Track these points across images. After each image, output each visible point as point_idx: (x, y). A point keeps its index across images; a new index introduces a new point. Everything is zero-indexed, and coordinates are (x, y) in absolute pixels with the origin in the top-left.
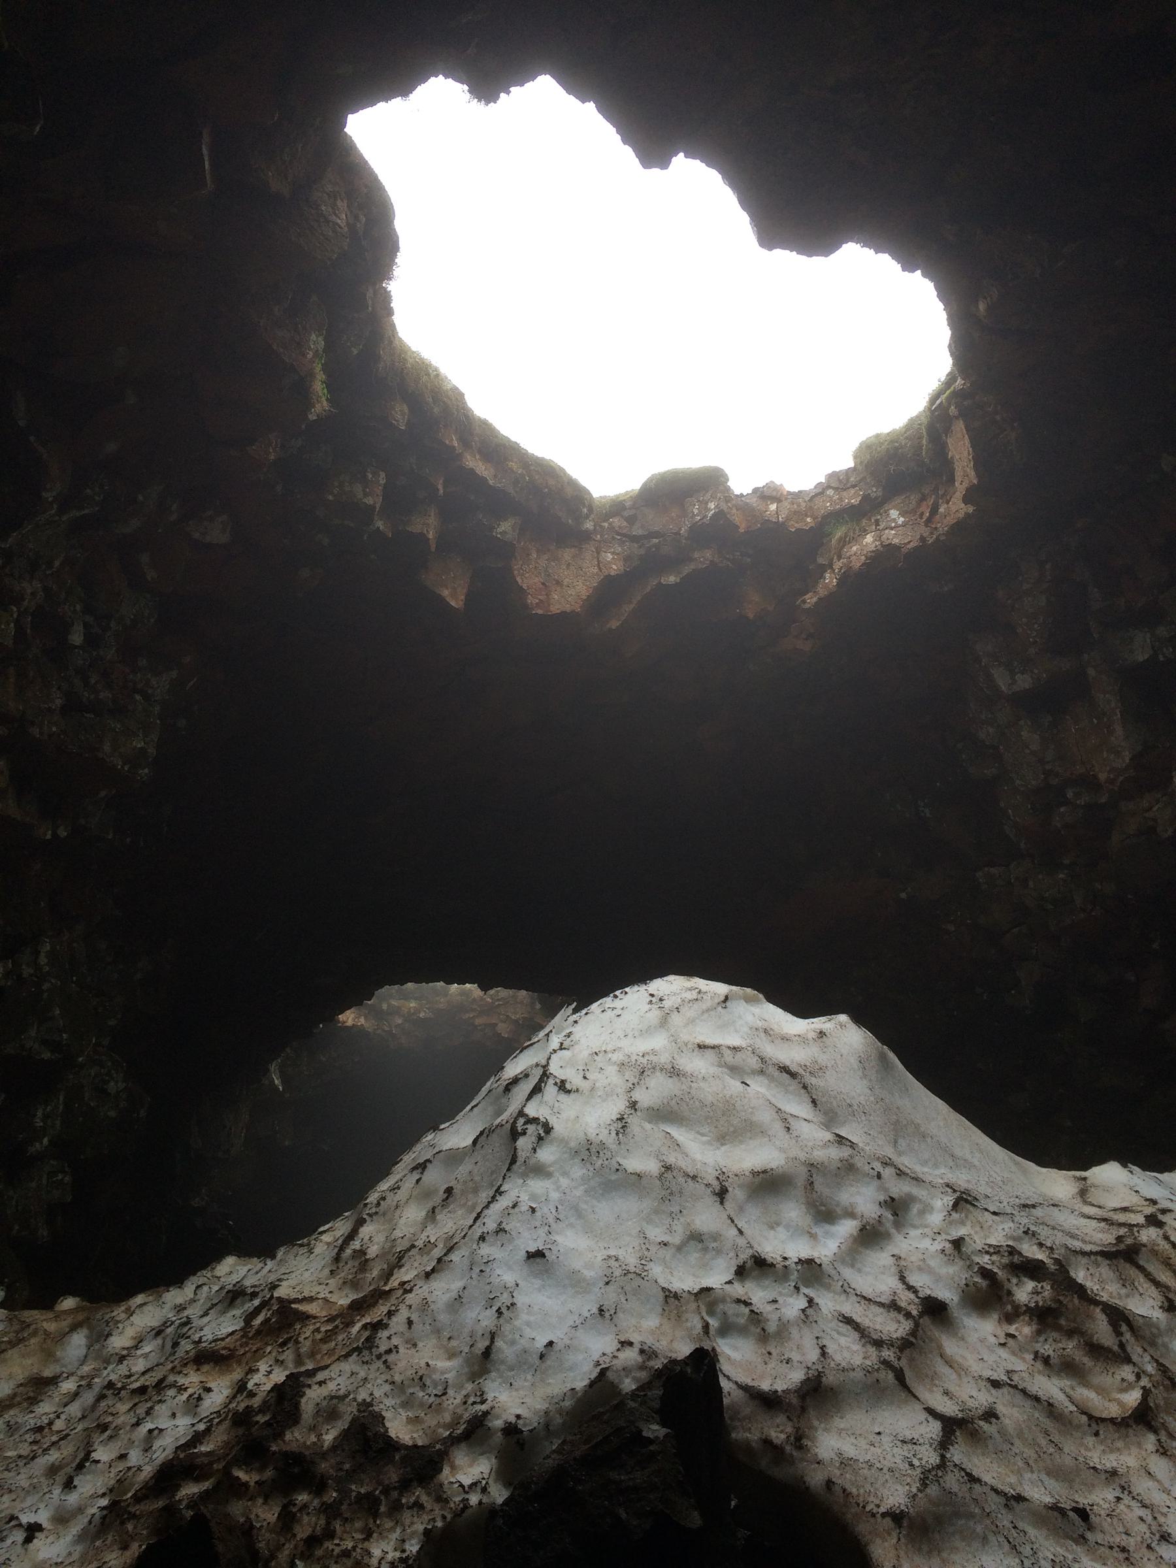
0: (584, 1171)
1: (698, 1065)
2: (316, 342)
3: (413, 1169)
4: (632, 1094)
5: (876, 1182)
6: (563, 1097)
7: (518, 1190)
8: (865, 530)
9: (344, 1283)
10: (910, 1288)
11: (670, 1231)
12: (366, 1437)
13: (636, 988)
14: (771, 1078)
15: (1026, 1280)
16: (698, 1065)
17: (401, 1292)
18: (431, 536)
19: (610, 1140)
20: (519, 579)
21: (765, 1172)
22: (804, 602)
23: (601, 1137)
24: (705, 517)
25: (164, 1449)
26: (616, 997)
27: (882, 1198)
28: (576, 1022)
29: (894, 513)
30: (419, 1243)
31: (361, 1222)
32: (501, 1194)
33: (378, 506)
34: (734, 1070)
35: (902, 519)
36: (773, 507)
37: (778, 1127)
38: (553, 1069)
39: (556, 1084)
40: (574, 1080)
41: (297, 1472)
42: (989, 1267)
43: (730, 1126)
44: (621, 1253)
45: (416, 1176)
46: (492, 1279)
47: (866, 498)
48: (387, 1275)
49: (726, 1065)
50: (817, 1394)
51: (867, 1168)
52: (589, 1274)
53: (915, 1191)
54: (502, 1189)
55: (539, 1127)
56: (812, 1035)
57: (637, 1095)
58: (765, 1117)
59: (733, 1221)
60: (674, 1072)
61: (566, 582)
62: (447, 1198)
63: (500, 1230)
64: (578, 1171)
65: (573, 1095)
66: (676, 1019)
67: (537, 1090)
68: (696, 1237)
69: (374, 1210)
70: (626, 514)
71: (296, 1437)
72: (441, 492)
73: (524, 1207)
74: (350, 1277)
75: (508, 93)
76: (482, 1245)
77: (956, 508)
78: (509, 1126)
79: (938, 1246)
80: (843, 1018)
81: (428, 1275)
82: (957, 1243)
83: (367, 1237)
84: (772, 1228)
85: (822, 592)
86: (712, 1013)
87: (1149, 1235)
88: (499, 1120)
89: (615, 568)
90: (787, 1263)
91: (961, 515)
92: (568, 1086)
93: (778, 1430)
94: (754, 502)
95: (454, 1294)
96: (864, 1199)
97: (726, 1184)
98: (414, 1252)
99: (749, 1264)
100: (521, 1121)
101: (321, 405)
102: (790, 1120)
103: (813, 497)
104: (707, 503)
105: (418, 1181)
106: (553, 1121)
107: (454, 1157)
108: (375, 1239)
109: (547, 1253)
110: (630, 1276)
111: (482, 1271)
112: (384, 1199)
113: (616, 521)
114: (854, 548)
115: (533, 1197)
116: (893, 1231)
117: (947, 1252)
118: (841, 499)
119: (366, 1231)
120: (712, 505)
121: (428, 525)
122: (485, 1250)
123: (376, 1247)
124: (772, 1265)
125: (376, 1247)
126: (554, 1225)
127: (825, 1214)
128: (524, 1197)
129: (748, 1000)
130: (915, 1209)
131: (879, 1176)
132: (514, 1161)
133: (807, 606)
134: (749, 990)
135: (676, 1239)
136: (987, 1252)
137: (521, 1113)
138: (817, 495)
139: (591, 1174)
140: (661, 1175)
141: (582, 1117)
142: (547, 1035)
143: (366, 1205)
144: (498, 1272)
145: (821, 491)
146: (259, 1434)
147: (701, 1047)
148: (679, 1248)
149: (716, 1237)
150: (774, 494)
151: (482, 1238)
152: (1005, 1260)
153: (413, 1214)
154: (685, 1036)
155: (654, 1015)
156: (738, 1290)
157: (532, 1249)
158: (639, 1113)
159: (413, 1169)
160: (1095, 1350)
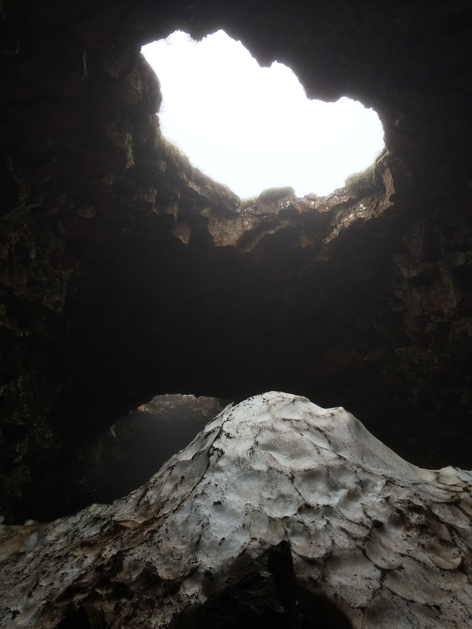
2: (129, 137)
4: (256, 439)
5: (354, 474)
6: (228, 440)
7: (210, 477)
8: (350, 212)
9: (141, 514)
10: (368, 517)
11: (272, 493)
13: (258, 396)
14: (312, 433)
15: (415, 514)
17: (163, 518)
18: (175, 215)
19: (247, 457)
20: (211, 233)
21: (310, 470)
22: (325, 241)
23: (243, 456)
24: (286, 207)
26: (250, 400)
27: (357, 481)
28: (233, 410)
29: (361, 205)
30: (171, 498)
31: (147, 490)
32: (204, 478)
34: (297, 429)
35: (365, 208)
36: (313, 203)
37: (315, 452)
38: (224, 428)
39: (225, 435)
40: (233, 433)
43: (296, 451)
44: (252, 503)
46: (200, 513)
47: (350, 199)
48: (158, 511)
49: (294, 427)
52: (239, 511)
53: (370, 478)
54: (204, 477)
55: (219, 452)
56: (328, 415)
57: (258, 439)
58: (310, 448)
59: (297, 490)
60: (273, 430)
61: (229, 233)
62: (182, 480)
63: (203, 493)
64: (234, 470)
65: (232, 439)
66: (274, 409)
67: (218, 437)
68: (282, 496)
69: (152, 485)
70: (253, 206)
72: (179, 197)
73: (213, 484)
74: (143, 512)
76: (196, 499)
77: (386, 203)
78: (207, 451)
79: (379, 500)
81: (174, 511)
82: (387, 499)
83: (150, 496)
84: (313, 493)
85: (333, 237)
88: (203, 449)
91: (389, 206)
92: (230, 436)
94: (305, 201)
95: (185, 519)
96: (350, 481)
97: (294, 475)
98: (168, 502)
99: (303, 507)
100: (212, 449)
101: (131, 162)
102: (320, 449)
105: (170, 474)
106: (224, 450)
107: (185, 464)
108: (153, 497)
109: (222, 503)
110: (255, 512)
112: (156, 481)
113: (250, 209)
114: (345, 220)
115: (216, 480)
118: (340, 200)
119: (149, 493)
120: (288, 202)
121: (174, 211)
122: (197, 501)
123: (153, 500)
124: (313, 508)
125: (153, 500)
126: (225, 492)
127: (334, 487)
129: (303, 401)
130: (370, 485)
131: (356, 472)
132: (209, 465)
134: (303, 397)
135: (274, 497)
136: (399, 503)
137: (212, 446)
138: (330, 198)
139: (240, 471)
141: (236, 448)
142: (222, 415)
143: (149, 483)
144: (202, 510)
147: (284, 420)
148: (275, 501)
149: (290, 496)
150: (313, 198)
151: (196, 497)
152: (406, 506)
155: (265, 407)
156: (299, 517)
157: (216, 501)
158: (259, 446)
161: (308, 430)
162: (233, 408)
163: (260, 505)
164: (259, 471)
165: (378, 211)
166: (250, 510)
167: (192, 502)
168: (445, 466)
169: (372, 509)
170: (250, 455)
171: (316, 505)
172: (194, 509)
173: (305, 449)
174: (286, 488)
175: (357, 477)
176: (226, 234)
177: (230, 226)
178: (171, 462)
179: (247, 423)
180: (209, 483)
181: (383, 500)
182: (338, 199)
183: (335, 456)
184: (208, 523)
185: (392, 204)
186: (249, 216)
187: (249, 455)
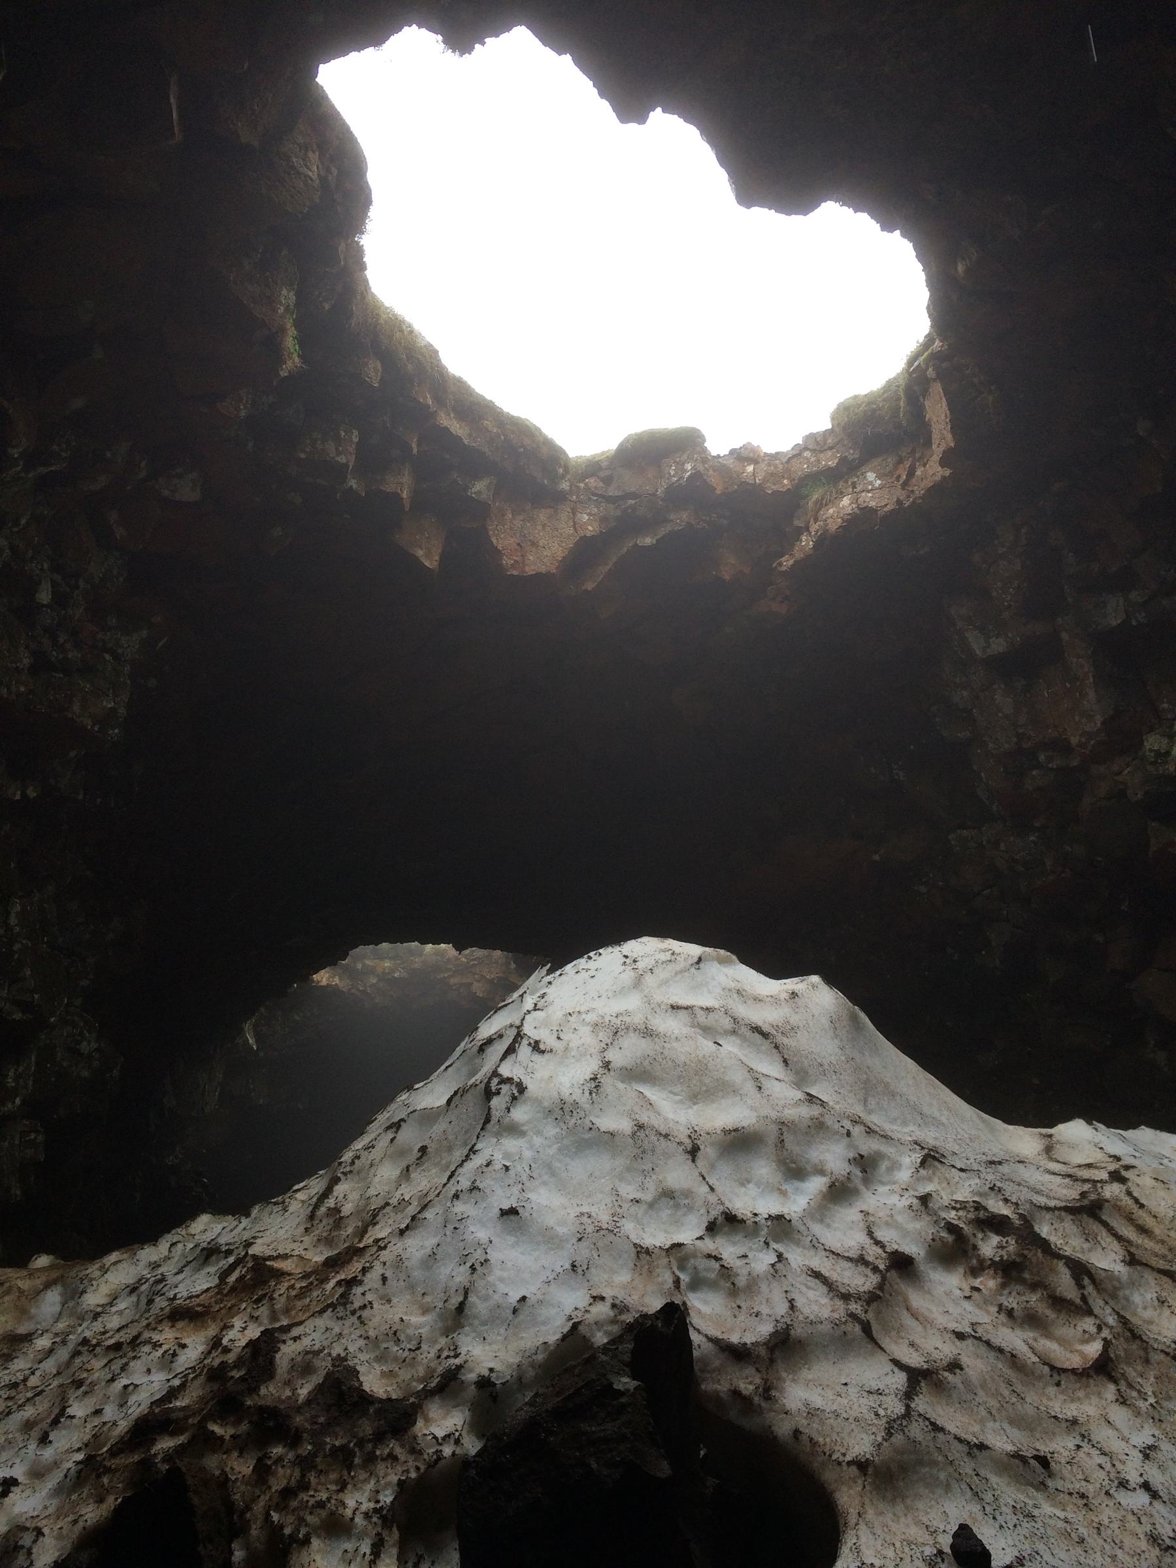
1: (672, 1025)
2: (287, 296)
3: (388, 1128)
5: (846, 1140)
6: (537, 1057)
7: (492, 1149)
8: (842, 493)
10: (877, 1243)
11: (642, 1188)
13: (610, 949)
14: (744, 1039)
15: (992, 1235)
16: (672, 1025)
17: (375, 1249)
18: (405, 495)
19: (584, 1100)
20: (494, 541)
21: (736, 1130)
22: (780, 564)
23: (574, 1097)
24: (681, 478)
26: (590, 958)
27: (851, 1155)
28: (550, 983)
29: (871, 476)
30: (394, 1201)
34: (706, 1030)
35: (879, 482)
36: (750, 468)
37: (750, 1087)
38: (527, 1029)
39: (530, 1044)
40: (547, 1038)
43: (702, 1085)
44: (593, 1210)
45: (390, 1135)
47: (843, 460)
48: (362, 1232)
49: (699, 1026)
51: (837, 1126)
52: (561, 1230)
54: (476, 1148)
55: (513, 1087)
56: (784, 996)
57: (611, 1055)
58: (738, 1077)
59: (704, 1179)
60: (648, 1033)
62: (421, 1157)
64: (552, 1130)
65: (547, 1056)
67: (511, 1050)
68: (668, 1194)
69: (348, 1169)
70: (602, 474)
72: (415, 451)
73: (497, 1166)
74: (325, 1234)
75: (483, 44)
76: (456, 1202)
77: (932, 471)
78: (483, 1085)
79: (905, 1202)
80: (815, 979)
81: (402, 1232)
82: (925, 1199)
84: (743, 1185)
85: (799, 555)
86: (686, 974)
87: (1112, 1191)
88: (473, 1080)
89: (591, 529)
90: (757, 1219)
91: (938, 478)
92: (542, 1047)
94: (730, 462)
95: (428, 1251)
96: (834, 1157)
98: (388, 1209)
100: (495, 1081)
101: (293, 361)
102: (762, 1079)
103: (790, 459)
105: (392, 1140)
106: (527, 1081)
107: (429, 1117)
108: (350, 1197)
109: (520, 1210)
110: (602, 1232)
113: (592, 482)
114: (831, 511)
115: (507, 1155)
116: (862, 1188)
118: (818, 461)
119: (340, 1189)
120: (688, 466)
121: (402, 485)
122: (460, 1208)
124: (743, 1221)
126: (527, 1184)
127: (795, 1171)
128: (498, 1158)
130: (883, 1166)
131: (849, 1134)
132: (487, 1120)
133: (783, 569)
134: (722, 952)
135: (648, 1197)
136: (954, 1208)
137: (495, 1073)
138: (794, 456)
140: (634, 1133)
141: (556, 1077)
142: (522, 996)
143: (340, 1164)
144: (472, 1229)
145: (798, 453)
147: (675, 1008)
149: (687, 1194)
151: (456, 1196)
152: (971, 1216)
154: (658, 997)
155: (628, 976)
156: (709, 1245)
157: (506, 1206)
158: (612, 1073)
159: (388, 1128)
162: (549, 978)
163: (613, 1215)
165: (912, 491)
166: (590, 1229)
168: (1067, 1119)
169: (887, 1224)
171: (750, 1215)
172: (450, 1227)
173: (727, 1078)
175: (851, 1146)
177: (544, 526)
178: (394, 1111)
179: (584, 1016)
182: (813, 459)
183: (799, 1095)
185: (947, 472)
187: (587, 1093)
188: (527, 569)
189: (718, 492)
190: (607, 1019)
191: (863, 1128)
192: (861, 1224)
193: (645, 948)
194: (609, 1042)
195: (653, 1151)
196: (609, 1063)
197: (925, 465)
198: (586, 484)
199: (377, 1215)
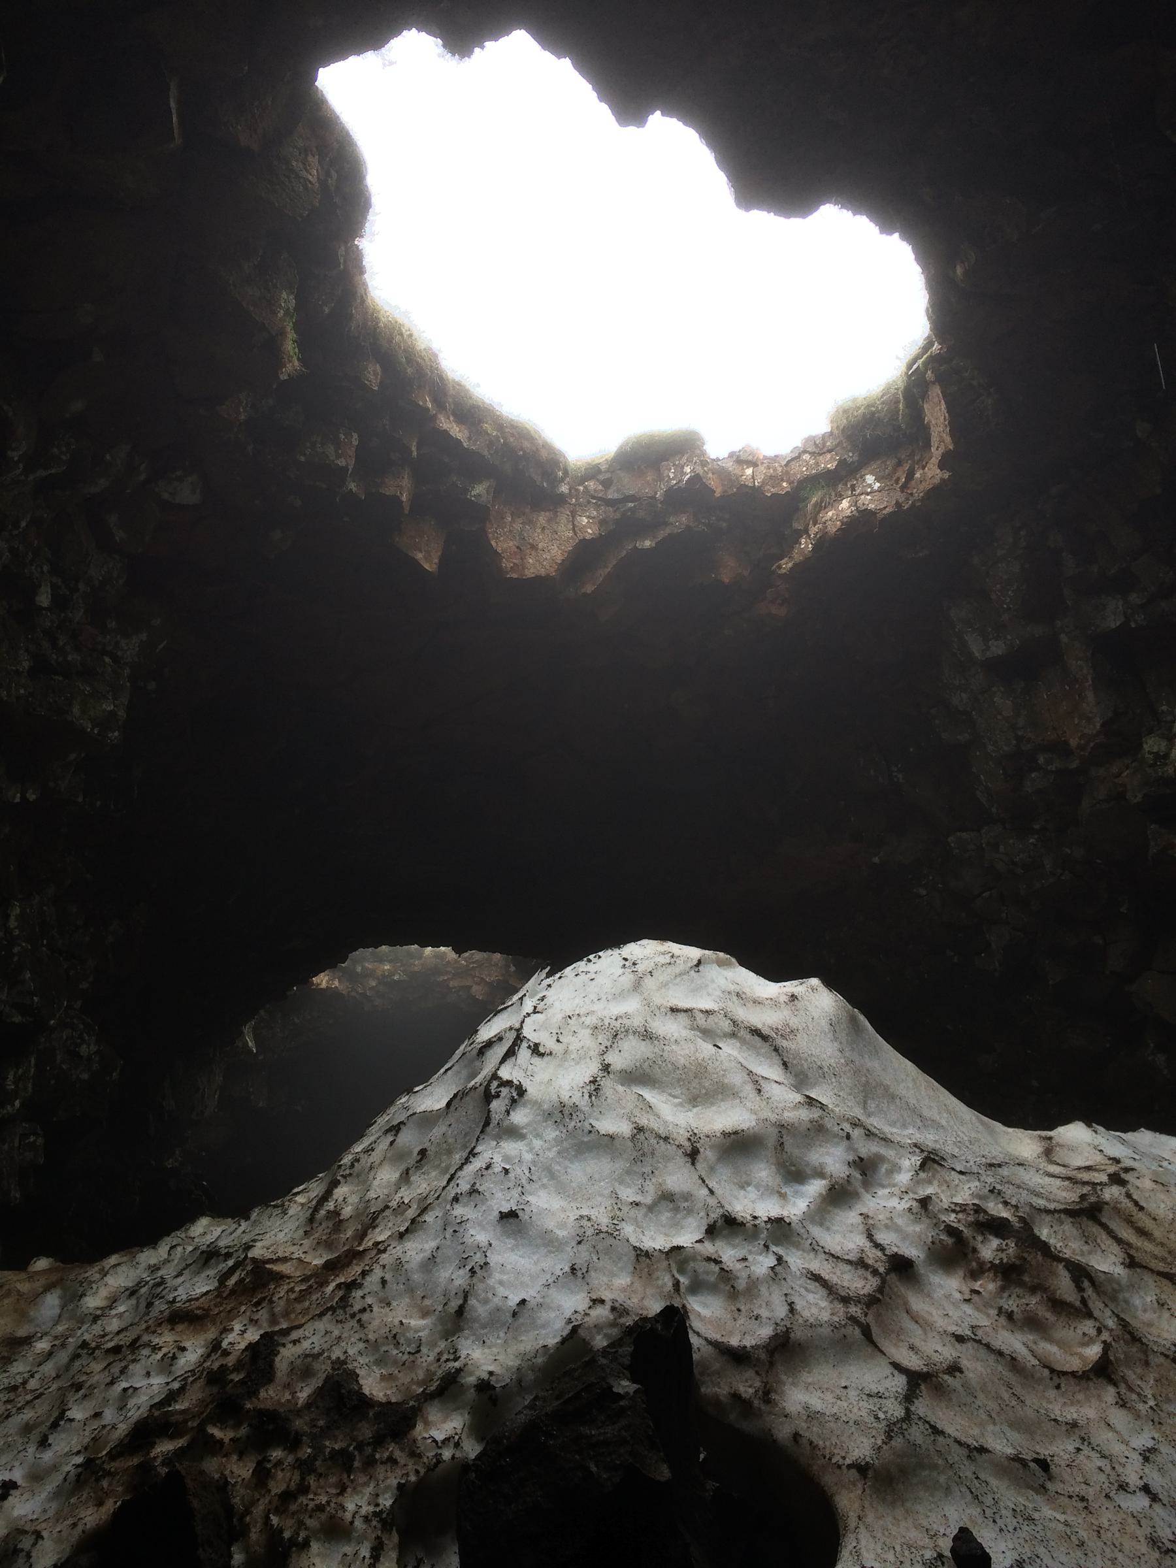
0: (558, 1133)
1: (671, 1028)
2: (287, 300)
3: (387, 1131)
5: (845, 1143)
6: (536, 1060)
7: (491, 1152)
8: (841, 496)
11: (642, 1191)
12: (340, 1395)
13: (609, 952)
14: (743, 1041)
15: (991, 1237)
16: (671, 1028)
17: (374, 1252)
18: (404, 498)
19: (583, 1103)
20: (493, 543)
21: (736, 1133)
22: (780, 567)
23: (573, 1100)
24: (680, 481)
25: (139, 1406)
26: (589, 961)
28: (549, 986)
29: (870, 479)
30: (393, 1204)
31: (335, 1184)
32: (475, 1155)
33: (351, 468)
34: (706, 1033)
35: (878, 485)
36: (749, 471)
37: (749, 1089)
38: (526, 1032)
39: (529, 1047)
40: (548, 1043)
41: (271, 1429)
42: (955, 1225)
43: (702, 1088)
44: (593, 1213)
47: (842, 463)
48: (361, 1236)
49: (698, 1029)
50: (786, 1350)
51: (836, 1129)
52: (561, 1233)
54: (476, 1151)
55: (513, 1090)
56: (783, 998)
57: (610, 1058)
58: (736, 1079)
59: (704, 1181)
60: (647, 1035)
62: (421, 1160)
64: (551, 1133)
65: (546, 1058)
67: (511, 1053)
68: (667, 1198)
69: (348, 1172)
70: (601, 477)
71: (270, 1396)
72: (415, 454)
73: (497, 1168)
74: (324, 1237)
75: (483, 47)
76: (456, 1206)
77: (931, 473)
78: (482, 1088)
79: (905, 1205)
80: (815, 981)
81: (401, 1236)
82: (924, 1202)
83: (341, 1199)
84: (742, 1188)
85: (797, 557)
86: (685, 977)
87: (1112, 1193)
88: (473, 1083)
90: (757, 1222)
91: (937, 481)
92: (541, 1050)
93: (746, 1385)
95: (428, 1254)
96: (833, 1159)
98: (388, 1212)
100: (495, 1083)
101: (292, 365)
102: (762, 1082)
104: (683, 467)
105: (392, 1143)
106: (526, 1084)
107: (428, 1119)
108: (350, 1200)
109: (520, 1213)
110: (602, 1235)
111: (455, 1231)
112: (358, 1160)
113: (591, 485)
114: (830, 514)
115: (507, 1159)
116: (861, 1190)
117: (914, 1211)
118: (817, 464)
119: (340, 1192)
120: (688, 469)
121: (401, 487)
122: (459, 1211)
124: (742, 1224)
126: (527, 1187)
127: (795, 1174)
128: (497, 1159)
129: (721, 964)
130: (883, 1169)
131: (848, 1137)
132: (487, 1123)
133: (784, 571)
134: (721, 954)
135: (648, 1200)
136: (954, 1211)
137: (495, 1076)
140: (634, 1136)
141: (554, 1080)
142: (521, 999)
143: (340, 1166)
144: (472, 1232)
146: (233, 1390)
147: (674, 1010)
148: (651, 1208)
149: (687, 1197)
151: (456, 1199)
152: (971, 1219)
153: (387, 1176)
154: (658, 1000)
155: (628, 979)
156: (709, 1248)
157: (505, 1210)
158: (611, 1076)
159: (387, 1131)
160: (1058, 1305)
161: (733, 1035)
164: (611, 1137)
165: (912, 494)
166: (590, 1232)
167: (447, 1213)
170: (590, 1096)
171: (749, 1218)
172: (450, 1230)
173: (726, 1081)
174: (678, 1177)
175: (851, 1148)
176: (533, 547)
177: (543, 529)
180: (488, 1167)
181: (915, 1204)
183: (798, 1098)
184: (486, 1264)
186: (589, 502)
187: (586, 1096)
188: (526, 572)
189: (717, 495)
190: (606, 1022)
191: (862, 1131)
192: (861, 1227)
193: (644, 950)
194: (609, 1044)
195: (653, 1154)
196: (608, 1065)
197: (924, 468)
198: (585, 487)
199: (377, 1218)
